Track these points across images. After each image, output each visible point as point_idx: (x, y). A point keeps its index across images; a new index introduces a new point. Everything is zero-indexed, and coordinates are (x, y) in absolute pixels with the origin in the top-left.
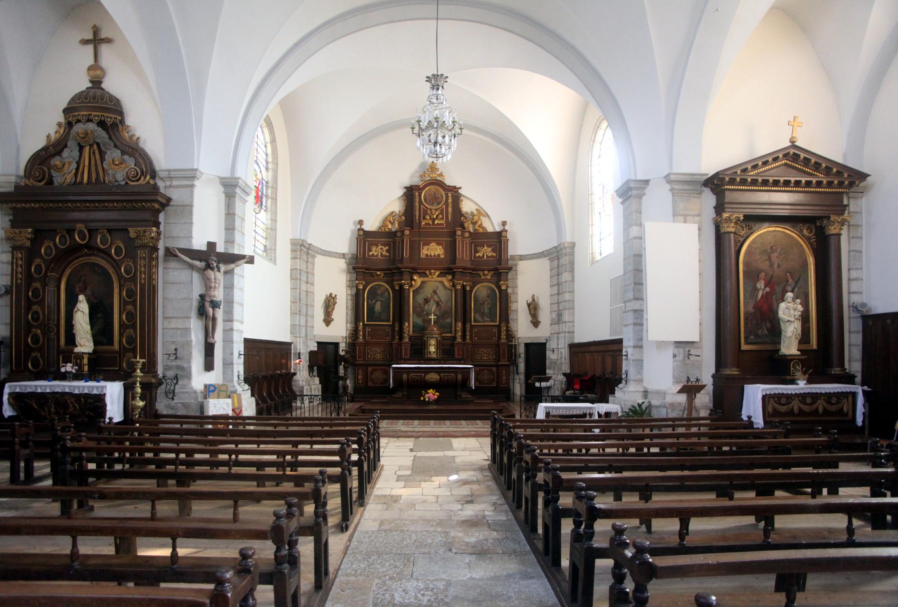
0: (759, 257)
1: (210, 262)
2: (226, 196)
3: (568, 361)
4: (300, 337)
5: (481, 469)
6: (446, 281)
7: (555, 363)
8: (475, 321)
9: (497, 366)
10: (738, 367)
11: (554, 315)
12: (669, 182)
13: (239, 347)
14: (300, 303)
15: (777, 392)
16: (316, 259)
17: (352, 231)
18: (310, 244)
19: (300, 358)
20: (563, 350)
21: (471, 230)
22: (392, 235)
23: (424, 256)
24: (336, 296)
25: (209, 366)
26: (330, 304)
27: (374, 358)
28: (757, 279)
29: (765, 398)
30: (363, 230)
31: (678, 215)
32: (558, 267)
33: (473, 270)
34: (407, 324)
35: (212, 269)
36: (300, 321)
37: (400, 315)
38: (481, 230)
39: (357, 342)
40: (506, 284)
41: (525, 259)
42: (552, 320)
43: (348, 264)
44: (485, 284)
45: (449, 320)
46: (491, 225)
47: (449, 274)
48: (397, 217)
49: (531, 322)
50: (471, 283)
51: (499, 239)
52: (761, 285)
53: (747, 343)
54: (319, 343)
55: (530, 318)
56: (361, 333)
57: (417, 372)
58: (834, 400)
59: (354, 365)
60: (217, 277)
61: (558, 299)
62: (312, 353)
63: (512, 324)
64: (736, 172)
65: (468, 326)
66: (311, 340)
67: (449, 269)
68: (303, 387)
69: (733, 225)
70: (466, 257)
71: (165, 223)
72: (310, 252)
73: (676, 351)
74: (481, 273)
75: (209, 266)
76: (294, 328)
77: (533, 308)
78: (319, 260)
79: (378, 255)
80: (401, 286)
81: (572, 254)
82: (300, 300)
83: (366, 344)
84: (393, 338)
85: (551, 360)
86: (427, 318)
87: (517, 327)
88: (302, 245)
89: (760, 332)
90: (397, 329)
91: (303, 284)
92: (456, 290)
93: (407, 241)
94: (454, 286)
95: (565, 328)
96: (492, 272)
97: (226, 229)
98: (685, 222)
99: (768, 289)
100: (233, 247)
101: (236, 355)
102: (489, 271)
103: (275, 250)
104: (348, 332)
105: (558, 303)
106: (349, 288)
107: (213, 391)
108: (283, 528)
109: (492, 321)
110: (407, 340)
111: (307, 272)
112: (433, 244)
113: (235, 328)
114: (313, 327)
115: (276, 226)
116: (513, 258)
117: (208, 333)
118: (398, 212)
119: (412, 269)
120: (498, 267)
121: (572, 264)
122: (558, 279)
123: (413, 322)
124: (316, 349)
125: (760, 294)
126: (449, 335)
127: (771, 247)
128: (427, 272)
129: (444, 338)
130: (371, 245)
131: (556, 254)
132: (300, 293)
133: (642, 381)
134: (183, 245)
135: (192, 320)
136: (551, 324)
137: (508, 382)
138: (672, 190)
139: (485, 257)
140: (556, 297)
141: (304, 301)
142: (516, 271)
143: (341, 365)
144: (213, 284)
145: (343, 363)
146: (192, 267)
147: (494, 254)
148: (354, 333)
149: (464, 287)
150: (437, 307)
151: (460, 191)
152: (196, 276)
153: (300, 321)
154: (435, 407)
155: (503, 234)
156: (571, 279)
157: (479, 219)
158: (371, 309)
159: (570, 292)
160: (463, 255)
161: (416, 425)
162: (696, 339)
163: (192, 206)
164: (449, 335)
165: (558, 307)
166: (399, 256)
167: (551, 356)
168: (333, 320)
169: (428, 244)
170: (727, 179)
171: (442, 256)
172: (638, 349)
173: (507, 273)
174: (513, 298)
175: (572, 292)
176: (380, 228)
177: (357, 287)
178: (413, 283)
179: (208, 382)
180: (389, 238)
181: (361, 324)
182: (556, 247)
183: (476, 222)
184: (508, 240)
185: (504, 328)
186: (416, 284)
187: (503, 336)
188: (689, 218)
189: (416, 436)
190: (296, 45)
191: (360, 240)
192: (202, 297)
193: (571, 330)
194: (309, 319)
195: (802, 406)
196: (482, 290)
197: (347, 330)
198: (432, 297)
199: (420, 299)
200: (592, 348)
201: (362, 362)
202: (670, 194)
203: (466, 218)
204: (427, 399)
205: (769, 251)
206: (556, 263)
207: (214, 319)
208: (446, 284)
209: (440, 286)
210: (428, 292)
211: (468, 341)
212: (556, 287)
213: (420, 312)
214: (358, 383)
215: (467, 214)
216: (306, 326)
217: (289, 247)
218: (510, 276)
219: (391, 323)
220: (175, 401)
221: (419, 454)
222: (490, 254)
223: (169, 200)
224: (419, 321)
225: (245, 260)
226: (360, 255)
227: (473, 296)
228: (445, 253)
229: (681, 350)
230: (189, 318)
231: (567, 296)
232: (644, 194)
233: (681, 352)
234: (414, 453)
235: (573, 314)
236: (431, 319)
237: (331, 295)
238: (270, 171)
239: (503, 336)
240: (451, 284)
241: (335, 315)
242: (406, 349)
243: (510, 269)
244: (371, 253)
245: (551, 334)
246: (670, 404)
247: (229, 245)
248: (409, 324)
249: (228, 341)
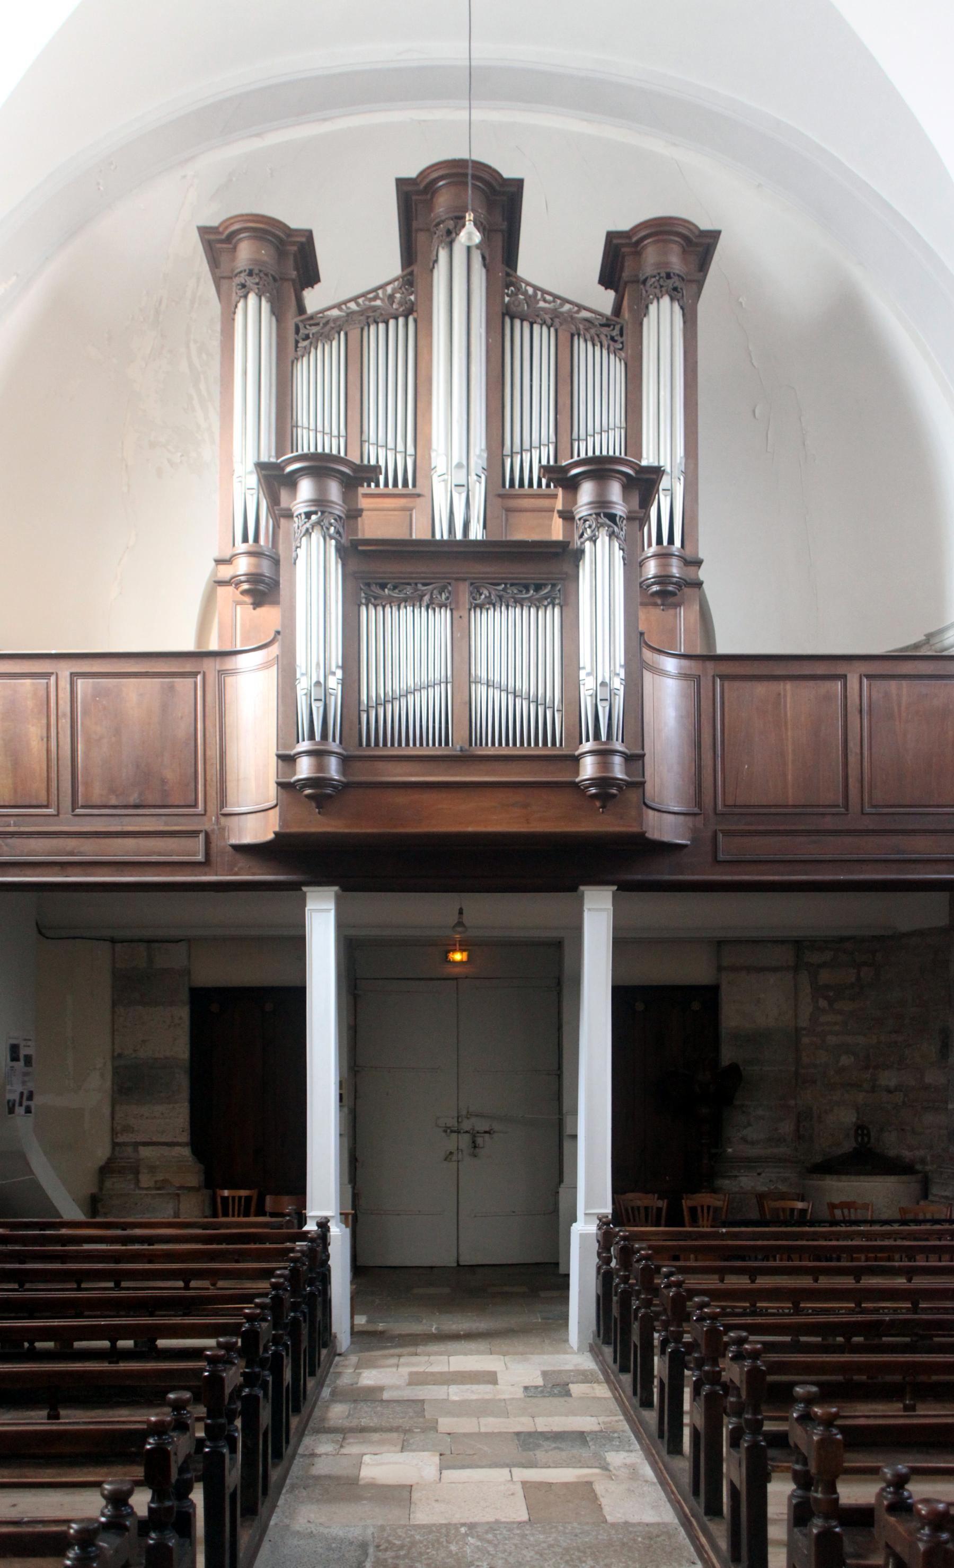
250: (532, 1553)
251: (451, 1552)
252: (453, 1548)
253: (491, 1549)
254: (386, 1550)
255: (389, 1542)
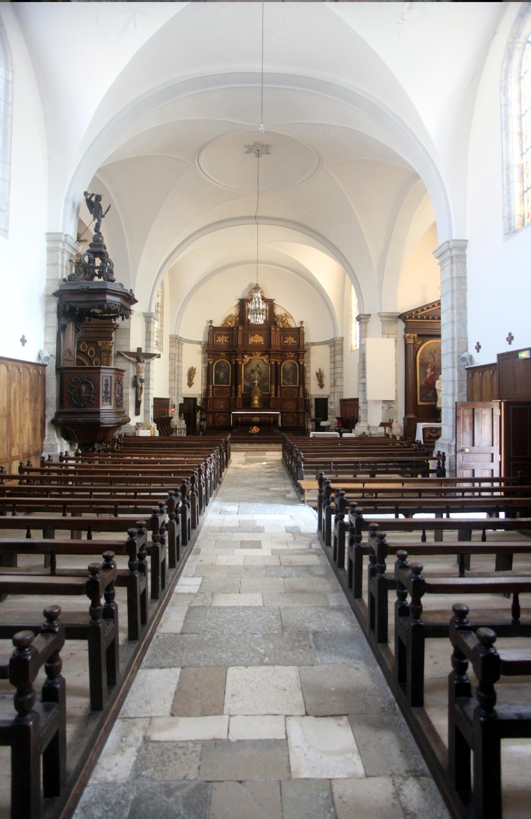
0: (427, 356)
1: (140, 358)
2: (146, 322)
3: (339, 410)
4: (175, 395)
5: (278, 461)
6: (265, 359)
7: (333, 411)
8: (283, 384)
9: (297, 413)
10: (414, 414)
11: (332, 381)
12: (380, 316)
13: (152, 403)
14: (175, 374)
15: (430, 427)
16: (183, 346)
17: (206, 327)
18: (180, 337)
19: (174, 408)
20: (336, 403)
21: (281, 326)
22: (231, 329)
23: (251, 343)
24: (195, 368)
25: (137, 413)
26: (191, 373)
27: (219, 408)
28: (427, 367)
29: (424, 429)
30: (212, 326)
31: (385, 334)
32: (334, 351)
33: (282, 352)
34: (240, 386)
35: (141, 362)
36: (174, 385)
37: (236, 380)
38: (287, 327)
39: (208, 397)
40: (303, 361)
41: (315, 345)
42: (331, 384)
43: (203, 348)
44: (290, 361)
45: (266, 384)
46: (294, 324)
47: (267, 354)
48: (234, 317)
49: (319, 385)
50: (280, 360)
51: (298, 332)
52: (429, 370)
53: (421, 401)
54: (184, 398)
55: (318, 383)
56: (211, 392)
57: (247, 416)
58: (434, 431)
59: (207, 412)
60: (142, 366)
61: (334, 371)
62: (181, 405)
63: (307, 386)
64: (412, 313)
65: (279, 387)
66: (180, 396)
67: (267, 350)
68: (176, 426)
69: (412, 340)
70: (278, 344)
71: (115, 338)
72: (180, 342)
73: (383, 405)
74: (287, 354)
75: (139, 361)
76: (171, 390)
77: (320, 376)
78: (186, 346)
79: (222, 342)
80: (236, 362)
81: (342, 344)
82: (175, 372)
83: (214, 398)
84: (231, 395)
85: (331, 409)
86: (252, 382)
87: (310, 388)
88: (177, 338)
89: (428, 395)
90: (234, 389)
91: (177, 362)
92: (271, 365)
93: (240, 334)
94: (270, 362)
95: (338, 389)
96: (294, 353)
97: (146, 340)
98: (388, 337)
99: (432, 373)
100: (150, 349)
101: (151, 407)
102: (292, 352)
103: (162, 343)
104: (203, 391)
105: (334, 374)
106: (203, 363)
107: (141, 426)
108: (98, 583)
109: (294, 384)
110: (240, 396)
111: (179, 355)
112: (257, 336)
113: (150, 392)
114: (181, 388)
115: (163, 329)
116: (308, 344)
117: (137, 396)
118: (234, 315)
119: (243, 351)
120: (298, 350)
121: (342, 350)
122: (334, 359)
123: (244, 385)
124: (183, 402)
125: (428, 375)
126: (267, 393)
127: (435, 351)
128: (253, 353)
129: (263, 395)
130: (218, 335)
131: (332, 344)
132: (175, 368)
133: (367, 421)
134: (124, 349)
135: (130, 389)
136: (331, 387)
137: (304, 422)
138: (381, 320)
139: (290, 344)
140: (333, 370)
141: (177, 373)
142: (309, 352)
143: (198, 412)
144: (141, 370)
145: (199, 411)
146: (130, 361)
147: (295, 342)
148: (207, 392)
149: (276, 362)
150: (259, 375)
151: (274, 302)
152: (131, 365)
153: (174, 385)
154: (257, 437)
155: (301, 329)
156: (341, 359)
157: (286, 319)
158: (217, 376)
159: (340, 367)
160: (276, 341)
161: (247, 446)
162: (394, 399)
163: (130, 329)
164: (267, 393)
165: (334, 376)
166: (235, 343)
167: (330, 407)
168: (193, 383)
169: (253, 335)
170: (407, 317)
171: (263, 343)
172: (365, 404)
173: (304, 354)
174: (307, 370)
175: (342, 367)
176: (223, 325)
177: (208, 362)
178: (244, 360)
179: (139, 421)
180: (228, 331)
181: (211, 386)
182: (333, 339)
183: (284, 321)
184: (304, 333)
185: (301, 389)
186: (246, 361)
187: (301, 394)
188: (390, 335)
189: (247, 451)
190: (184, 242)
191: (211, 333)
192: (135, 377)
193: (341, 391)
194: (179, 383)
195: (431, 434)
196: (287, 364)
197: (202, 390)
198: (256, 369)
199: (249, 370)
200: (350, 403)
201: (212, 410)
202: (381, 323)
203: (278, 319)
204: (253, 432)
205: (433, 352)
206: (333, 348)
207: (141, 388)
208: (265, 361)
209: (261, 362)
210: (253, 366)
211: (279, 397)
212: (333, 364)
213: (248, 378)
214: (209, 424)
215: (278, 316)
216: (178, 388)
217: (169, 340)
218: (306, 355)
219: (230, 385)
220: (121, 431)
221: (248, 457)
222: (293, 342)
223: (118, 326)
224: (248, 384)
225: (156, 357)
226: (211, 342)
227: (282, 368)
228: (265, 341)
229: (386, 405)
230: (128, 388)
231: (339, 370)
232: (369, 321)
233: (386, 406)
234: (245, 457)
235: (343, 381)
236: (255, 383)
237: (192, 368)
238: (160, 297)
239: (301, 394)
240: (268, 361)
241: (194, 381)
242: (239, 402)
243: (305, 351)
244: (217, 341)
245: (331, 393)
246: (379, 433)
247: (148, 348)
248: (241, 387)
249: (147, 400)
250: (232, 642)
251: (273, 643)
252: (271, 646)
253: (253, 644)
254: (305, 645)
255: (306, 650)
